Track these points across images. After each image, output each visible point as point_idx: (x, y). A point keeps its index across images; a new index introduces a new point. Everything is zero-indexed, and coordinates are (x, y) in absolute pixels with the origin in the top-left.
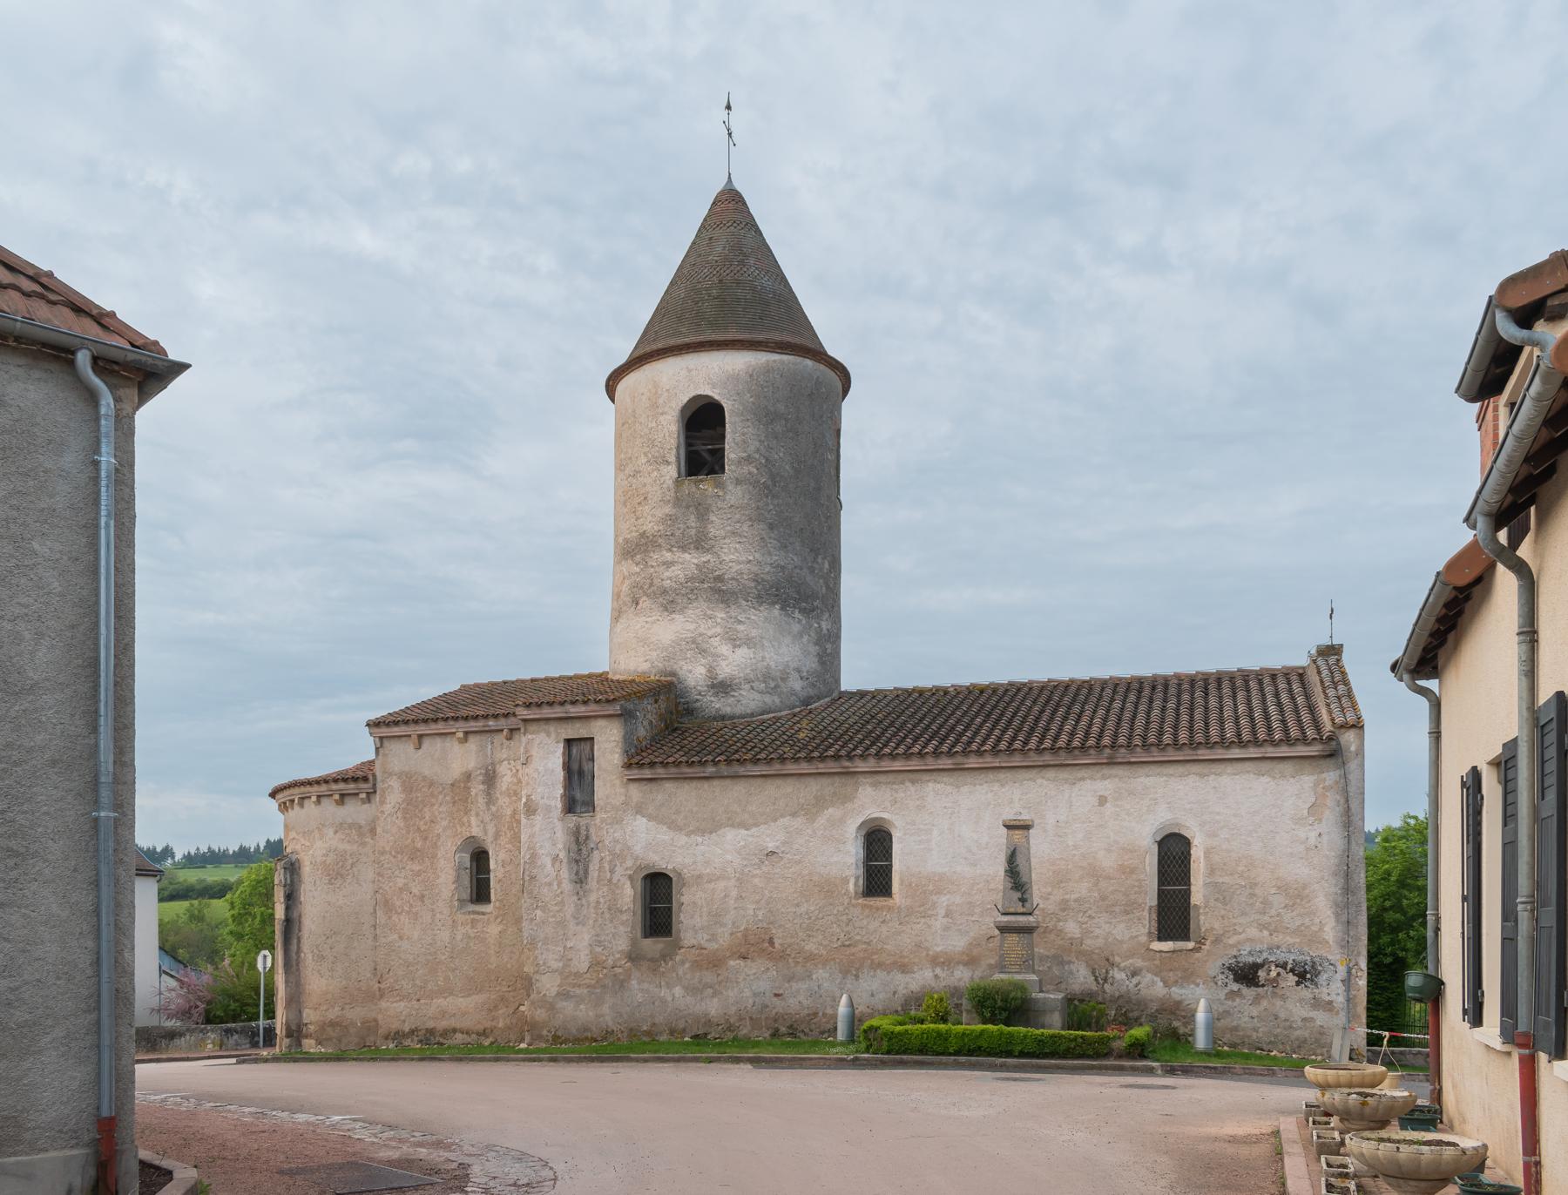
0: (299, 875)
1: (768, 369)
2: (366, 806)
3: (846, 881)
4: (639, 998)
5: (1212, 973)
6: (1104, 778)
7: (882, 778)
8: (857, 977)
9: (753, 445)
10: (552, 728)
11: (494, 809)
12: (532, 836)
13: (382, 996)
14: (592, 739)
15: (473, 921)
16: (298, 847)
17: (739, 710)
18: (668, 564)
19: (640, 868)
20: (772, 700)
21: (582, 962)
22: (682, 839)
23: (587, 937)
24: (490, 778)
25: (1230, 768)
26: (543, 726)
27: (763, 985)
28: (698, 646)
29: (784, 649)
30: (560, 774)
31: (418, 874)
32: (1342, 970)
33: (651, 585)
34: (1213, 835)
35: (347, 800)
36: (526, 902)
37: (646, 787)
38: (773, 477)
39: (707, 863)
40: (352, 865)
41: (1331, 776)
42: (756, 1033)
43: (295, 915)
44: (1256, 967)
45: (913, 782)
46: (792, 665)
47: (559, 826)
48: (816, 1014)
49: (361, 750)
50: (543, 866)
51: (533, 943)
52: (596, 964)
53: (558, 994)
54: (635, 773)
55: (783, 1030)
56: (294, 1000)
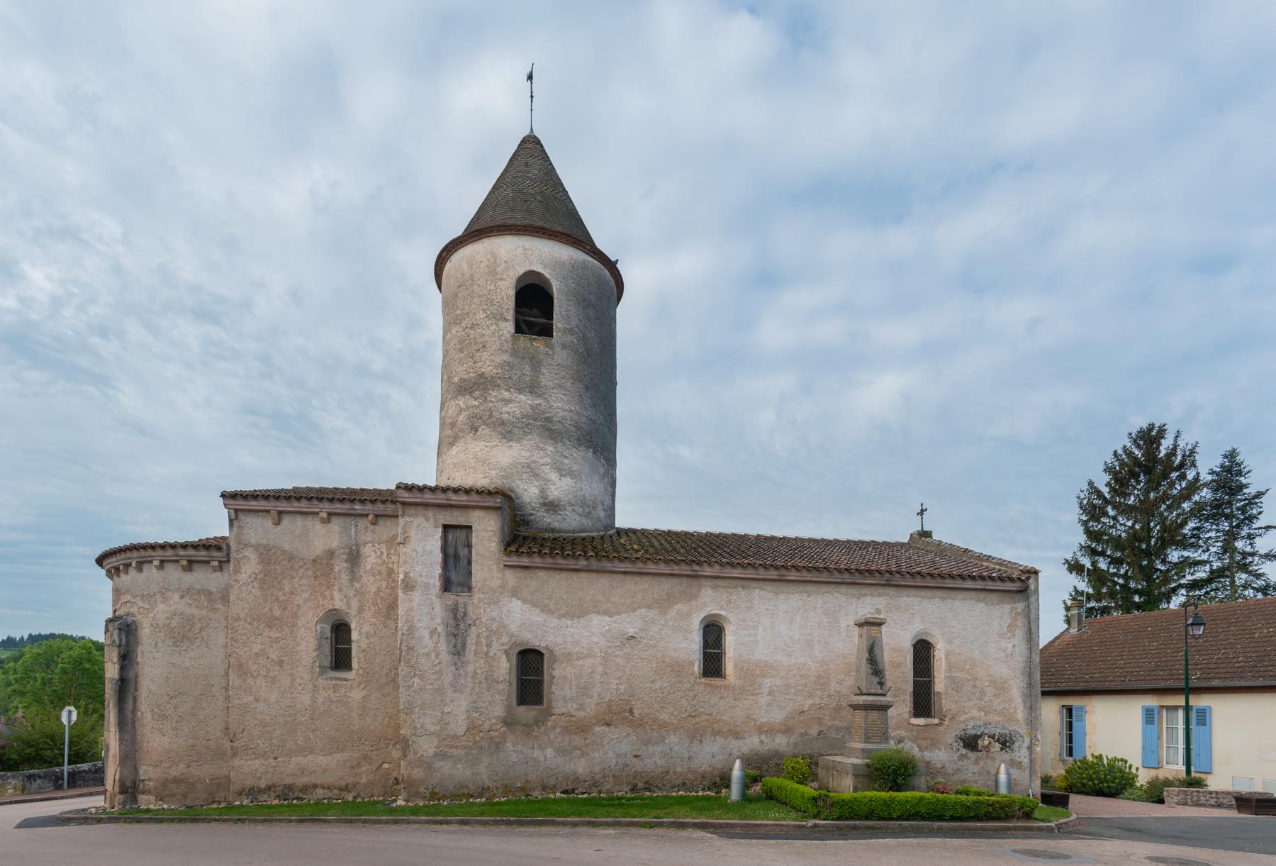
0: (136, 636)
1: (584, 266)
2: (218, 574)
3: (691, 663)
4: (514, 758)
5: (950, 741)
6: (880, 596)
7: (720, 582)
8: (701, 741)
9: (574, 322)
10: (430, 513)
11: (357, 585)
12: (410, 610)
13: (234, 755)
14: (470, 527)
15: (335, 686)
16: (134, 610)
17: (564, 526)
18: (507, 402)
19: (515, 644)
20: (586, 522)
21: (459, 725)
22: (553, 622)
23: (464, 703)
24: (354, 557)
25: (961, 595)
26: (421, 510)
27: (625, 748)
28: (533, 472)
29: (594, 485)
30: (438, 556)
31: (277, 640)
32: (1027, 740)
33: (491, 416)
34: (950, 642)
35: (195, 566)
36: (403, 669)
37: (522, 573)
38: (587, 350)
39: (576, 643)
40: (201, 630)
41: (1020, 606)
42: (618, 788)
43: (131, 674)
44: (977, 737)
45: (744, 588)
46: (599, 498)
47: (437, 602)
48: (668, 772)
49: (216, 524)
50: (421, 638)
51: (410, 708)
52: (473, 728)
53: (436, 755)
54: (514, 560)
55: (640, 785)
56: (130, 756)
